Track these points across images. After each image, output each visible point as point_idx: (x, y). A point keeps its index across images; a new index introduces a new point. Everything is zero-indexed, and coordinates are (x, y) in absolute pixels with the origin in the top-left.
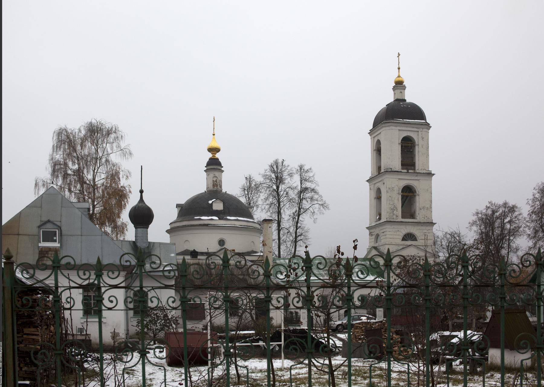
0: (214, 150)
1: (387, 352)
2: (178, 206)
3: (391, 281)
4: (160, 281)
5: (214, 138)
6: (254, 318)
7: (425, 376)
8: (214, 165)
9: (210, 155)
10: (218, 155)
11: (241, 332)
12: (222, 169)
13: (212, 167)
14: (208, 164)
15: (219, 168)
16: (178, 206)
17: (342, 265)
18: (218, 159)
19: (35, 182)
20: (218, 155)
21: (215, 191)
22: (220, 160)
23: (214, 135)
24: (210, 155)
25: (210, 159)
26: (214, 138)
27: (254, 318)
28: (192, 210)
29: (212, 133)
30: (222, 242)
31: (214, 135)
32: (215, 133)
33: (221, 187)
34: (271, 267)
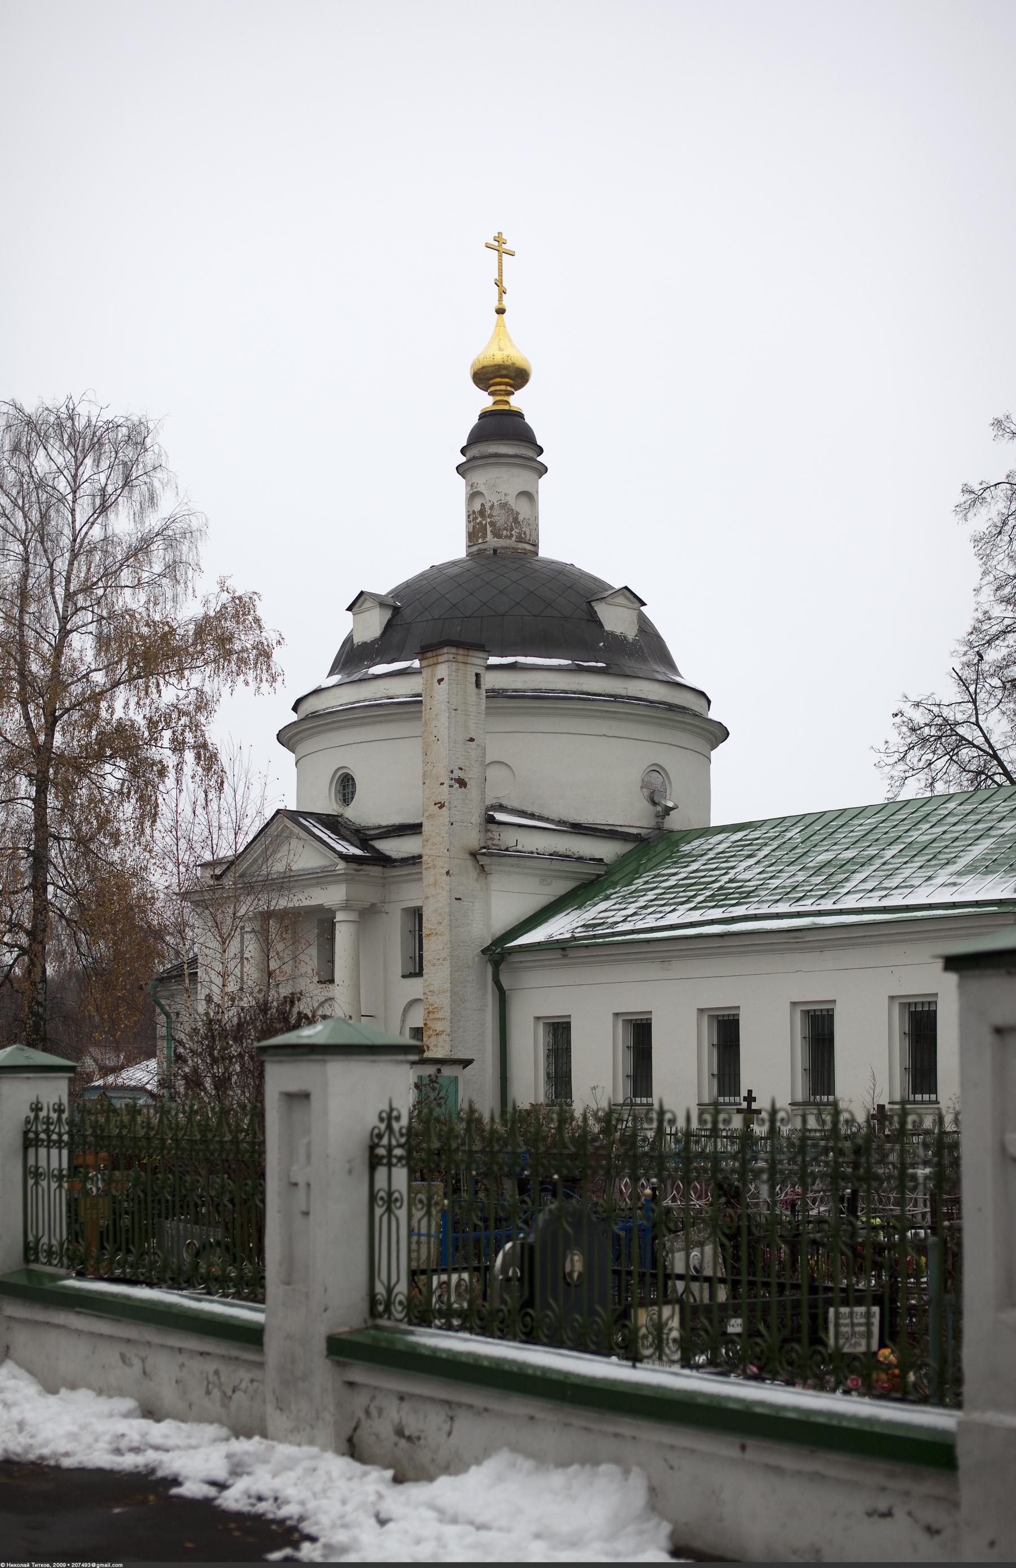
0: (501, 377)
3: (30, 587)
5: (500, 325)
6: (358, 852)
8: (502, 438)
9: (485, 401)
10: (518, 400)
11: (682, 1561)
14: (477, 437)
15: (530, 453)
17: (14, 679)
18: (520, 415)
19: (262, 623)
20: (518, 400)
23: (501, 311)
24: (485, 401)
25: (484, 415)
26: (500, 325)
27: (358, 852)
28: (418, 623)
29: (495, 304)
31: (501, 311)
32: (506, 303)
33: (536, 545)
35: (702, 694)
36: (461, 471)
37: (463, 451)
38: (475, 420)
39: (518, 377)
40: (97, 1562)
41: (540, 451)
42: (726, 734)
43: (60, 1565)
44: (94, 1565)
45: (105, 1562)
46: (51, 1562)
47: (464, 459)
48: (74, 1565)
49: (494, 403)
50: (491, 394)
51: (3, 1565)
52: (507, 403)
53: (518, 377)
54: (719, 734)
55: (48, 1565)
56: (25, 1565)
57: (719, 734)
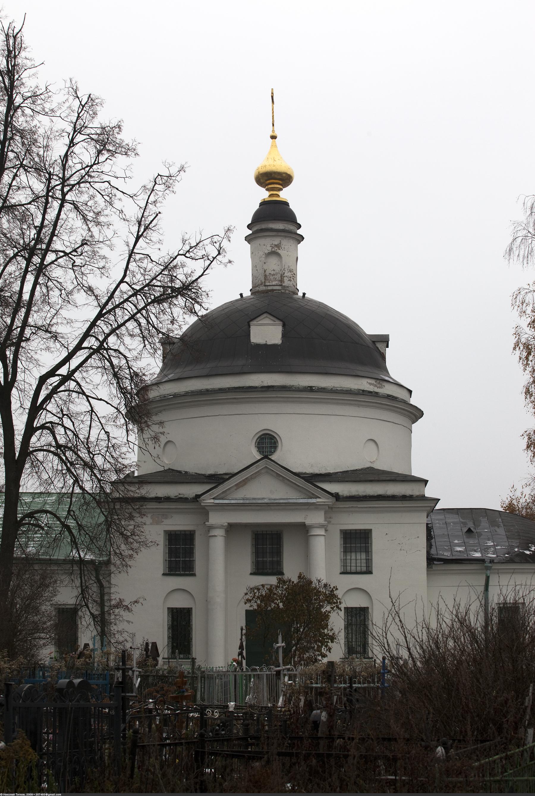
0: (274, 179)
1: (380, 677)
2: (385, 340)
4: (316, 534)
5: (274, 146)
7: (114, 508)
8: (274, 221)
9: (263, 194)
10: (285, 194)
12: (299, 232)
13: (264, 226)
15: (291, 227)
16: (385, 340)
18: (286, 204)
20: (285, 194)
21: (274, 297)
22: (291, 207)
23: (273, 137)
24: (263, 194)
25: (263, 204)
26: (274, 146)
30: (267, 443)
31: (273, 137)
32: (277, 133)
33: (294, 276)
34: (127, 487)
35: (302, 236)
36: (250, 228)
37: (249, 227)
38: (257, 207)
39: (283, 179)
40: (48, 793)
41: (299, 226)
42: (303, 238)
43: (30, 794)
44: (47, 794)
45: (52, 793)
46: (25, 793)
47: (250, 232)
48: (37, 794)
49: (270, 196)
50: (267, 190)
51: (1, 794)
52: (278, 196)
53: (283, 179)
54: (416, 414)
55: (24, 795)
56: (12, 795)
57: (416, 414)
